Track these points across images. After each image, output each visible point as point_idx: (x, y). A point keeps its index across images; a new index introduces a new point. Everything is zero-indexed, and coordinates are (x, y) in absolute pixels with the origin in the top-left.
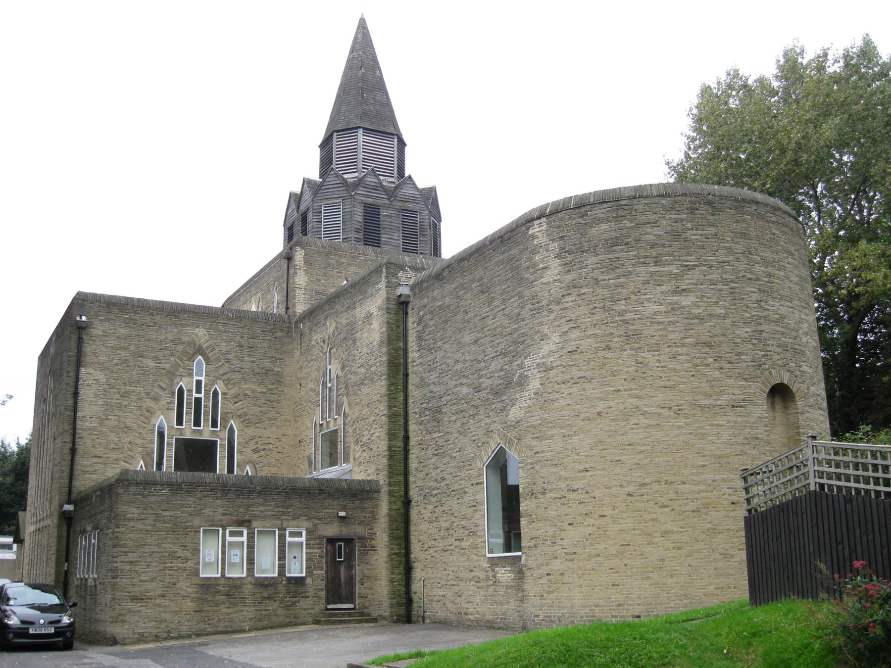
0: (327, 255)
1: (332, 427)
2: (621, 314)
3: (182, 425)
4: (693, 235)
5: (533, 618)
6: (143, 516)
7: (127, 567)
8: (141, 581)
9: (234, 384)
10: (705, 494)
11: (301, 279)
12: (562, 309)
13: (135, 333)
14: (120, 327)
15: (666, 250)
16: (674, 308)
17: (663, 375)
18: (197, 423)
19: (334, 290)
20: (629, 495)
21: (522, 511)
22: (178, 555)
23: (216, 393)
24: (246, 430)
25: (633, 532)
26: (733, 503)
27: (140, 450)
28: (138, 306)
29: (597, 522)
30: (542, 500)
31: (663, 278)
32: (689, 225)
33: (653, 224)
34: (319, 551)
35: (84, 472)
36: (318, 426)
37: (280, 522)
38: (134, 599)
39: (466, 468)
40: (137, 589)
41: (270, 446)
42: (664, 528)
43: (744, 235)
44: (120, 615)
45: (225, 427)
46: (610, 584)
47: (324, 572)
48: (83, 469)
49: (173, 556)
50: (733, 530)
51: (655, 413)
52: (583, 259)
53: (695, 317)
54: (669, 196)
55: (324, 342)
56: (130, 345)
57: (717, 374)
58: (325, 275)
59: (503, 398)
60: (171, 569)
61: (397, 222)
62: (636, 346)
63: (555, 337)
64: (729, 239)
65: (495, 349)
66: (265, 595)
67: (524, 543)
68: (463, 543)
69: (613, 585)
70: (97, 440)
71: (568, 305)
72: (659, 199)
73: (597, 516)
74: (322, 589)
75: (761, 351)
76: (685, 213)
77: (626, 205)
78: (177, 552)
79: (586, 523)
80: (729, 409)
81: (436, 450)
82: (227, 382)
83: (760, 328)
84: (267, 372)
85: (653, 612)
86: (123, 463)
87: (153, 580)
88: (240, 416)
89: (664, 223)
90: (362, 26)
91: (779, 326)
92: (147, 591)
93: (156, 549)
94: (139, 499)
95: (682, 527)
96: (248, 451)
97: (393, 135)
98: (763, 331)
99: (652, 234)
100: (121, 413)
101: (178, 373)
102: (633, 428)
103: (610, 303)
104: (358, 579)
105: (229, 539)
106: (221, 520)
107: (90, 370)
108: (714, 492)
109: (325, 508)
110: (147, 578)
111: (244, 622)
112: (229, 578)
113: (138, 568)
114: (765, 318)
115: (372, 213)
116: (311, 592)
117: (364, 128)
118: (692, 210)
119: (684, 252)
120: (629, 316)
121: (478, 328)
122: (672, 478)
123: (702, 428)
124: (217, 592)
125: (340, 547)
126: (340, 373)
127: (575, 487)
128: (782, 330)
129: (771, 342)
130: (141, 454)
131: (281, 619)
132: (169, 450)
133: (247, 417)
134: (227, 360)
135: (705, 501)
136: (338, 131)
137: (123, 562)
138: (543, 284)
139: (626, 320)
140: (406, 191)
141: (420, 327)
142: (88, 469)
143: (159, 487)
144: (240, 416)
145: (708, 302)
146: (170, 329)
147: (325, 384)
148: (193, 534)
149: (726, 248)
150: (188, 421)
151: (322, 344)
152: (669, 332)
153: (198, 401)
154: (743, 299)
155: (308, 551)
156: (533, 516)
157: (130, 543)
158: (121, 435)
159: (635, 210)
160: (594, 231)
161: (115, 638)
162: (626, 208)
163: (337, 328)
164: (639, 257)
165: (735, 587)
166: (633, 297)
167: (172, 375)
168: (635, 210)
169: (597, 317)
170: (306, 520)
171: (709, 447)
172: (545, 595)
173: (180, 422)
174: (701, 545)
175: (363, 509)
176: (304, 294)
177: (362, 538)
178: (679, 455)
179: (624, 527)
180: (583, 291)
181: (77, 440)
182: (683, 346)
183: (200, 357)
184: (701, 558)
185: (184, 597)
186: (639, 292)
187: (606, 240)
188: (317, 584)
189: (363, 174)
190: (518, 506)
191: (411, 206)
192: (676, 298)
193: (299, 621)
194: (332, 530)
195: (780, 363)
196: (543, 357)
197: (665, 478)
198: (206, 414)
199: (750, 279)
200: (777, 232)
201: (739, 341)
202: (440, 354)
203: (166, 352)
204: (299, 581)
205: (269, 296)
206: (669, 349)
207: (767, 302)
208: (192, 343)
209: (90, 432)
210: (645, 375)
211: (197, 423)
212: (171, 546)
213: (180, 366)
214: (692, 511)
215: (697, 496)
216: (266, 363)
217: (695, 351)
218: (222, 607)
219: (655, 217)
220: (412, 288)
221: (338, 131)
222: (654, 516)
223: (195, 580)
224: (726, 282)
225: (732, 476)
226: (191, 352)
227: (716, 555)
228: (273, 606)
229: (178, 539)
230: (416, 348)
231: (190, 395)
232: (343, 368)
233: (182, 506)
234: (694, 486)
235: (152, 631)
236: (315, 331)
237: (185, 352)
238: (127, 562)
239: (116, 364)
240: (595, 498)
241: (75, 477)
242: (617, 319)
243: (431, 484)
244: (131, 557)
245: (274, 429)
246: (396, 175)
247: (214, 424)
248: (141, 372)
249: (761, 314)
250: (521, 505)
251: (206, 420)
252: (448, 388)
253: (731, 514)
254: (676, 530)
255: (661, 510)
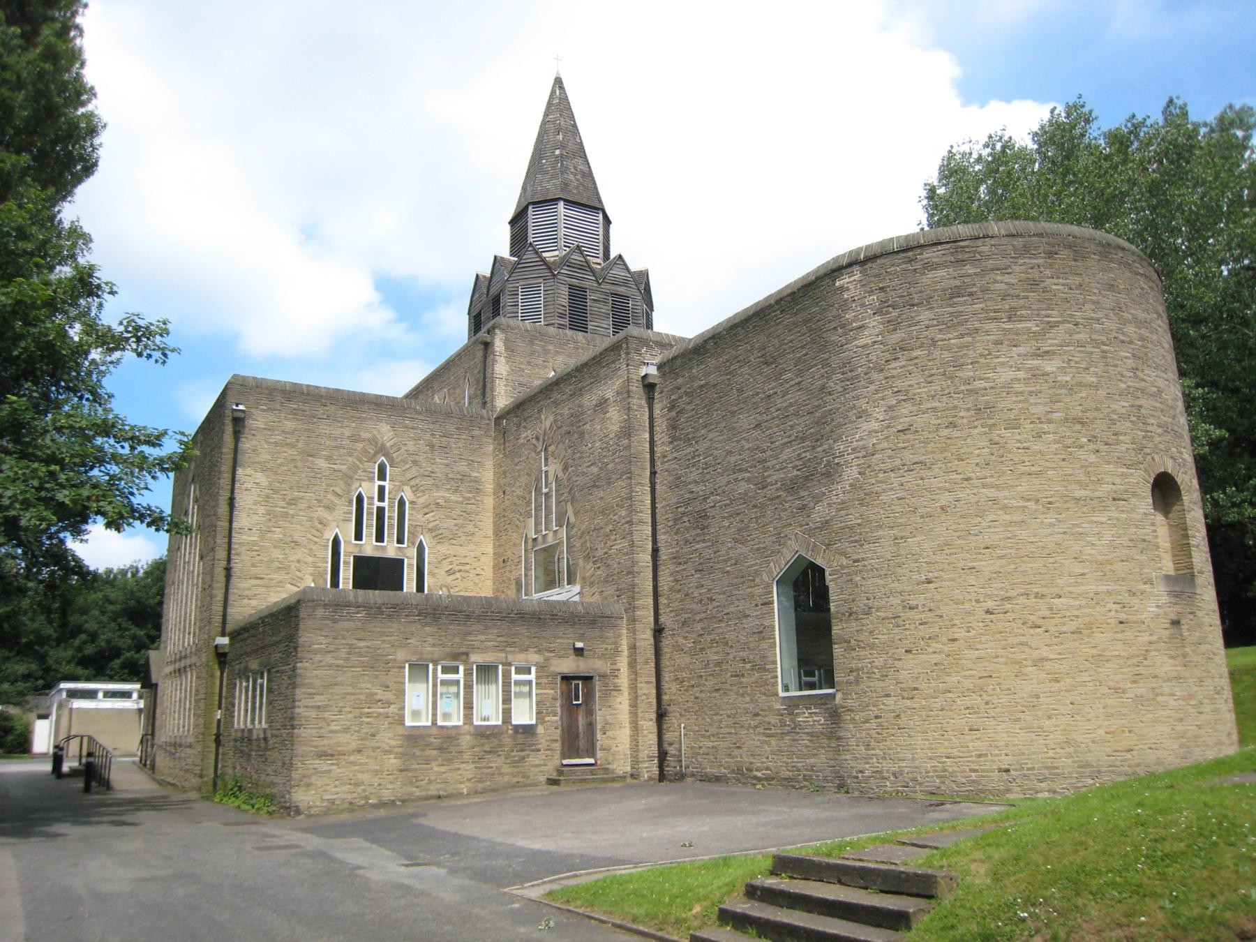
0: (531, 341)
1: (551, 540)
2: (967, 382)
3: (361, 540)
4: (1056, 286)
5: (855, 774)
6: (332, 648)
7: (313, 714)
8: (331, 732)
9: (423, 491)
10: (1087, 611)
11: (501, 367)
12: (886, 378)
13: (305, 427)
14: (286, 419)
15: (1022, 302)
16: (1035, 375)
17: (1026, 459)
18: (380, 537)
19: (540, 382)
20: (988, 612)
21: (834, 636)
22: (378, 697)
23: (402, 503)
24: (439, 547)
25: (996, 660)
26: (1121, 623)
27: (310, 570)
28: (308, 394)
29: (946, 648)
30: (864, 622)
31: (1020, 338)
32: (1048, 272)
33: (1005, 270)
34: (552, 691)
35: (242, 597)
36: (530, 541)
37: (504, 655)
38: (322, 755)
39: (746, 584)
40: (325, 742)
41: (468, 567)
42: (1036, 654)
43: (1111, 287)
44: (304, 776)
45: (413, 544)
46: (967, 728)
47: (557, 718)
48: (239, 592)
49: (372, 700)
50: (1124, 657)
51: (1018, 507)
52: (913, 314)
53: (1062, 386)
54: (1022, 236)
55: (538, 439)
56: (297, 441)
57: (1093, 458)
58: (529, 363)
59: (802, 493)
60: (368, 715)
61: (606, 309)
62: (990, 422)
63: (879, 413)
64: (1096, 291)
65: (788, 434)
66: (487, 748)
67: (839, 676)
68: (743, 680)
69: (971, 730)
70: (258, 558)
71: (895, 372)
72: (1010, 239)
73: (945, 640)
74: (556, 741)
75: (1141, 431)
76: (1042, 258)
77: (967, 247)
78: (376, 694)
79: (930, 650)
80: (1110, 503)
81: (701, 564)
82: (416, 489)
83: (1138, 403)
84: (464, 477)
85: (1026, 764)
86: (289, 586)
87: (346, 730)
88: (431, 530)
89: (1017, 269)
90: (558, 82)
91: (1157, 401)
92: (339, 744)
93: (350, 690)
94: (326, 625)
95: (1060, 654)
96: (441, 572)
97: (598, 209)
98: (1141, 407)
99: (1001, 283)
100: (287, 524)
101: (357, 477)
102: (990, 527)
103: (952, 369)
104: (599, 727)
105: (441, 676)
106: (432, 653)
107: (249, 471)
108: (1098, 609)
109: (559, 638)
110: (338, 728)
111: (461, 783)
112: (442, 727)
113: (326, 715)
114: (1143, 390)
115: (577, 296)
116: (543, 742)
117: (565, 200)
118: (1051, 254)
119: (1044, 306)
120: (978, 384)
121: (761, 409)
122: (1045, 591)
123: (1078, 526)
124: (427, 745)
125: (577, 686)
126: (560, 474)
127: (913, 603)
128: (1161, 406)
129: (1151, 421)
130: (311, 575)
131: (506, 778)
132: (346, 570)
133: (440, 532)
134: (415, 463)
135: (1088, 619)
136: (534, 203)
137: (306, 707)
138: (857, 347)
139: (973, 390)
140: (617, 272)
141: (674, 414)
142: (246, 593)
143: (353, 610)
144: (431, 530)
145: (1077, 368)
146: (346, 423)
147: (538, 490)
148: (397, 670)
149: (1093, 302)
150: (369, 535)
151: (534, 441)
152: (1031, 404)
153: (381, 511)
154: (1116, 366)
155: (539, 691)
156: (853, 642)
157: (317, 683)
158: (287, 551)
159: (979, 253)
160: (928, 278)
161: (297, 807)
162: (967, 250)
163: (555, 421)
164: (986, 311)
165: (1130, 732)
166: (982, 360)
167: (349, 479)
168: (979, 253)
169: (935, 387)
170: (536, 653)
171: (1088, 550)
172: (873, 743)
173: (358, 536)
174: (1084, 677)
175: (604, 639)
176: (505, 386)
177: (603, 676)
178: (1051, 560)
179: (983, 653)
180: (915, 354)
181: (232, 557)
182: (1050, 422)
183: (383, 458)
184: (1086, 694)
185: (386, 752)
186: (990, 354)
187: (944, 290)
188: (549, 734)
189: (564, 253)
190: (830, 630)
191: (621, 290)
192: (1036, 362)
193: (529, 781)
194: (568, 665)
195: (1162, 447)
196: (862, 439)
197: (1036, 590)
198: (391, 526)
199: (1123, 342)
200: (1146, 287)
201: (1115, 417)
202: (702, 446)
203: (342, 451)
204: (528, 730)
205: (458, 391)
206: (1032, 426)
207: (1143, 371)
208: (373, 441)
209: (248, 548)
210: (1003, 459)
211: (380, 537)
212: (369, 686)
213: (359, 468)
214: (1072, 633)
215: (1076, 613)
216: (462, 467)
217: (1065, 429)
218: (434, 764)
219: (1007, 261)
220: (660, 367)
221: (534, 203)
222: (1023, 639)
223: (400, 730)
224: (1097, 344)
225: (1118, 587)
226: (372, 452)
227: (1104, 690)
228: (497, 762)
229: (377, 677)
230: (666, 439)
231: (371, 503)
232: (565, 469)
233: (382, 634)
234: (1072, 600)
235: (345, 796)
236: (524, 427)
237: (365, 451)
238: (313, 707)
239: (281, 465)
240: (942, 617)
241: (230, 602)
242: (963, 388)
243: (694, 606)
244: (319, 700)
245: (472, 546)
246: (601, 255)
247: (400, 541)
248: (312, 474)
249: (1137, 385)
250: (834, 628)
251: (390, 535)
252: (716, 486)
253: (1120, 636)
254: (1052, 656)
255: (1032, 631)
